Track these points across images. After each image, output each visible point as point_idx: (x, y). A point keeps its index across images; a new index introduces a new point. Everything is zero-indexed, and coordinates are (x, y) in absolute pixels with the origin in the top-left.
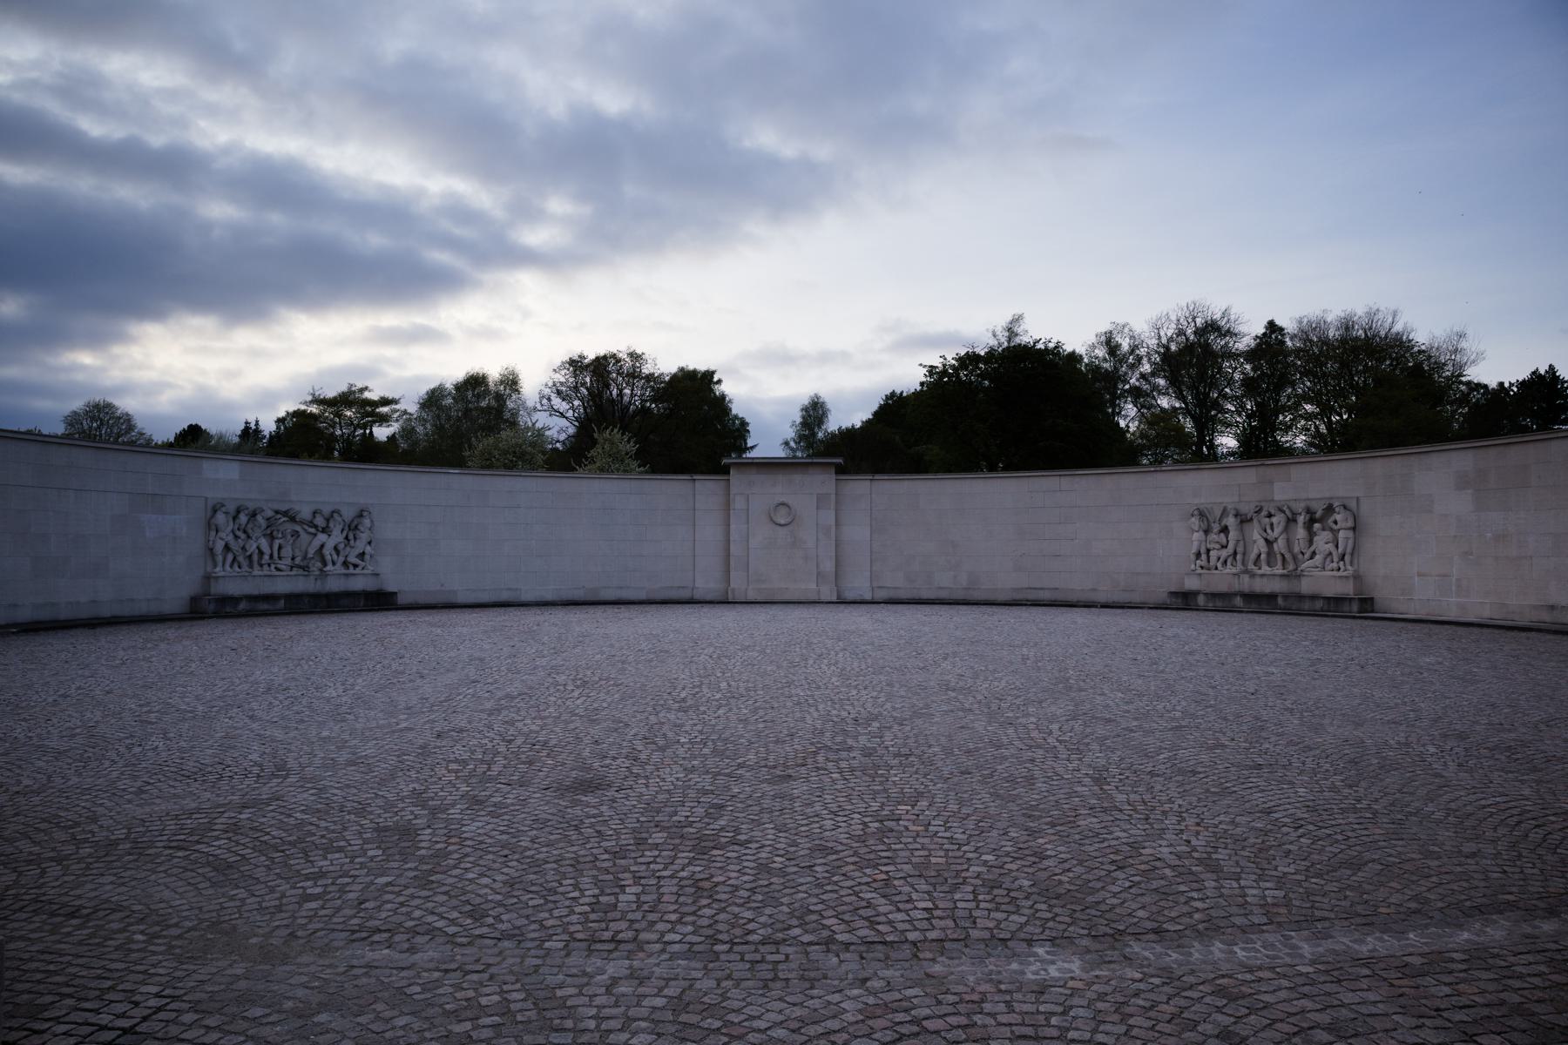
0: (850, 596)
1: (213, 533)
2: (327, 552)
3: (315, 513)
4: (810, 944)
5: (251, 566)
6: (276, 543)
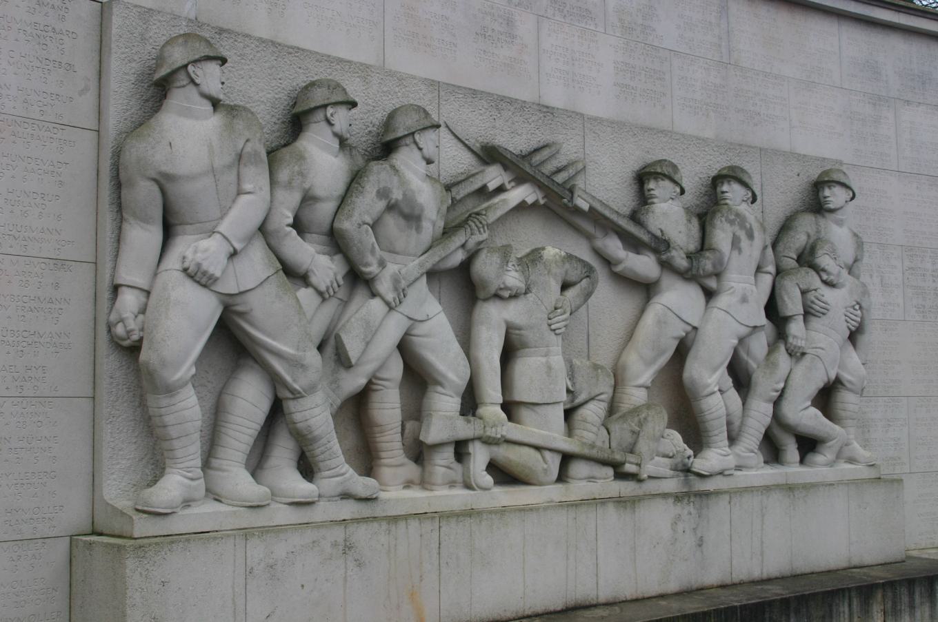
0: (900, 170)
1: (143, 237)
2: (708, 374)
3: (643, 178)
4: (933, 3)
5: (367, 458)
6: (492, 322)
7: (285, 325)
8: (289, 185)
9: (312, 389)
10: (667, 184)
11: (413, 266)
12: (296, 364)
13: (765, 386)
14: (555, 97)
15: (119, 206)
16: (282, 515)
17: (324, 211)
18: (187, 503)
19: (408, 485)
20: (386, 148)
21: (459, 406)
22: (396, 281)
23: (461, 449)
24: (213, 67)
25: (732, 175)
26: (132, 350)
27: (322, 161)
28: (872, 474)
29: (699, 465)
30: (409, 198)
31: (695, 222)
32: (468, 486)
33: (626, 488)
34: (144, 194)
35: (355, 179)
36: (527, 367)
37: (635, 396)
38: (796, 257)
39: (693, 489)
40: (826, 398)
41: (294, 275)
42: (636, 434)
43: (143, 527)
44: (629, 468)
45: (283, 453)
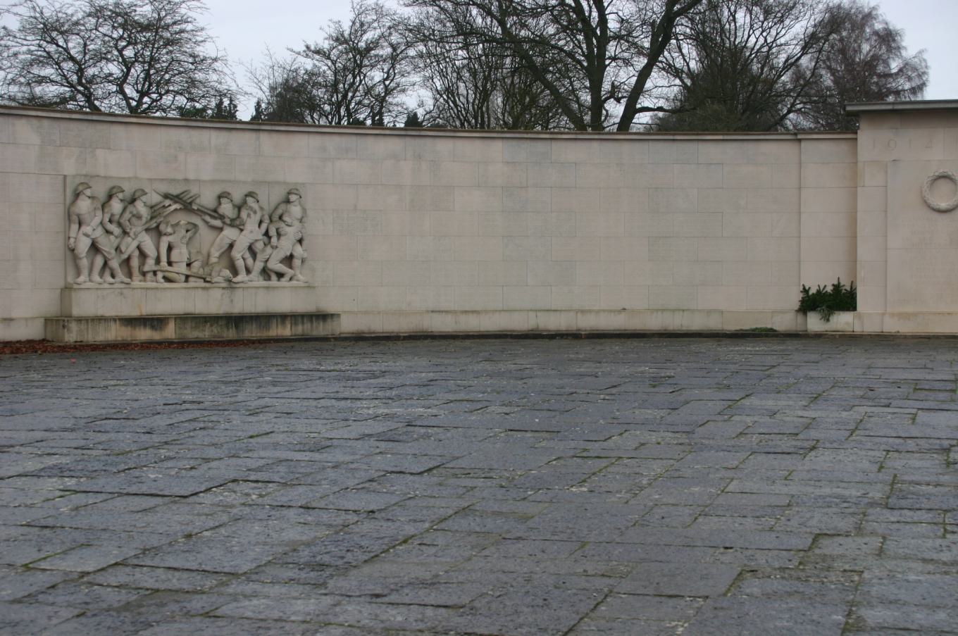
1: (75, 227)
2: (237, 254)
5: (130, 275)
7: (107, 244)
8: (107, 213)
9: (113, 259)
10: (226, 199)
11: (139, 229)
12: (109, 253)
13: (260, 257)
14: (191, 176)
15: (69, 219)
16: (106, 286)
17: (116, 218)
18: (85, 282)
19: (140, 281)
20: (133, 201)
21: (799, 304)
22: (135, 233)
23: (155, 273)
24: (88, 190)
25: (250, 194)
26: (73, 250)
27: (116, 206)
28: (306, 285)
29: (235, 280)
30: (138, 213)
31: (236, 209)
32: (157, 282)
33: (208, 285)
34: (75, 218)
35: (124, 209)
36: (175, 254)
37: (213, 260)
38: (276, 216)
39: (231, 285)
40: (289, 260)
41: (108, 232)
42: (211, 271)
43: (75, 286)
44: (208, 279)
45: (107, 273)
